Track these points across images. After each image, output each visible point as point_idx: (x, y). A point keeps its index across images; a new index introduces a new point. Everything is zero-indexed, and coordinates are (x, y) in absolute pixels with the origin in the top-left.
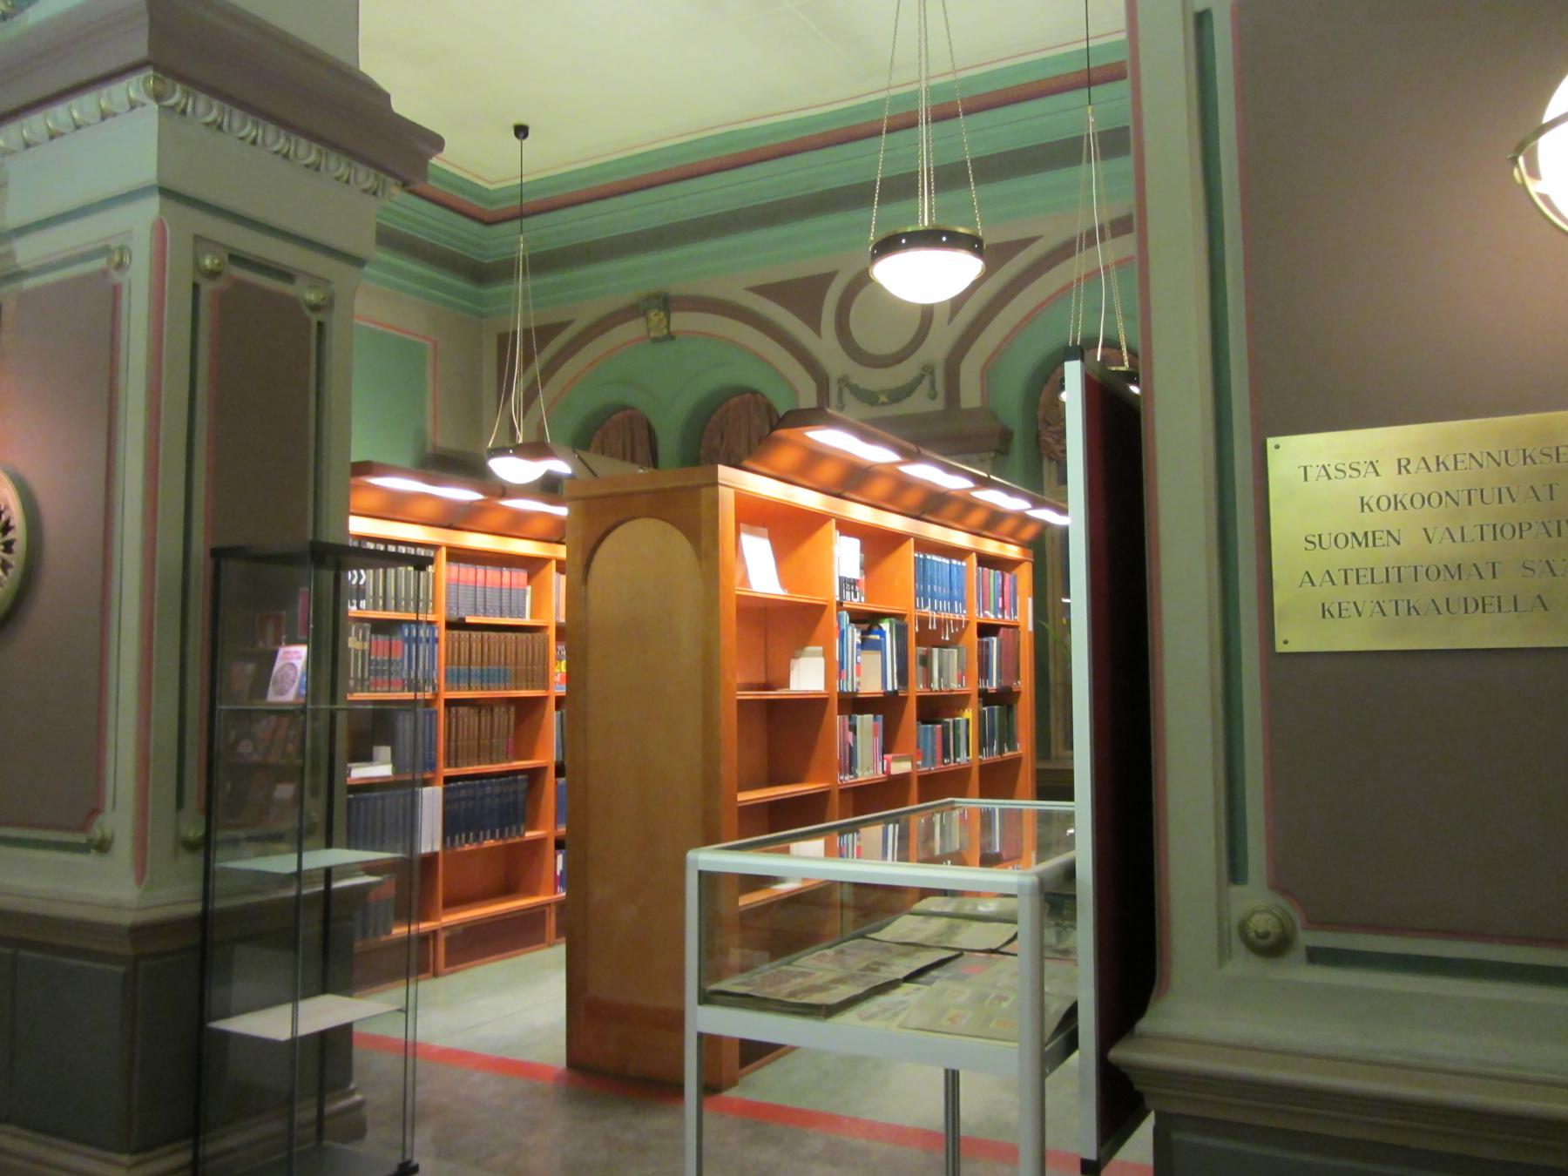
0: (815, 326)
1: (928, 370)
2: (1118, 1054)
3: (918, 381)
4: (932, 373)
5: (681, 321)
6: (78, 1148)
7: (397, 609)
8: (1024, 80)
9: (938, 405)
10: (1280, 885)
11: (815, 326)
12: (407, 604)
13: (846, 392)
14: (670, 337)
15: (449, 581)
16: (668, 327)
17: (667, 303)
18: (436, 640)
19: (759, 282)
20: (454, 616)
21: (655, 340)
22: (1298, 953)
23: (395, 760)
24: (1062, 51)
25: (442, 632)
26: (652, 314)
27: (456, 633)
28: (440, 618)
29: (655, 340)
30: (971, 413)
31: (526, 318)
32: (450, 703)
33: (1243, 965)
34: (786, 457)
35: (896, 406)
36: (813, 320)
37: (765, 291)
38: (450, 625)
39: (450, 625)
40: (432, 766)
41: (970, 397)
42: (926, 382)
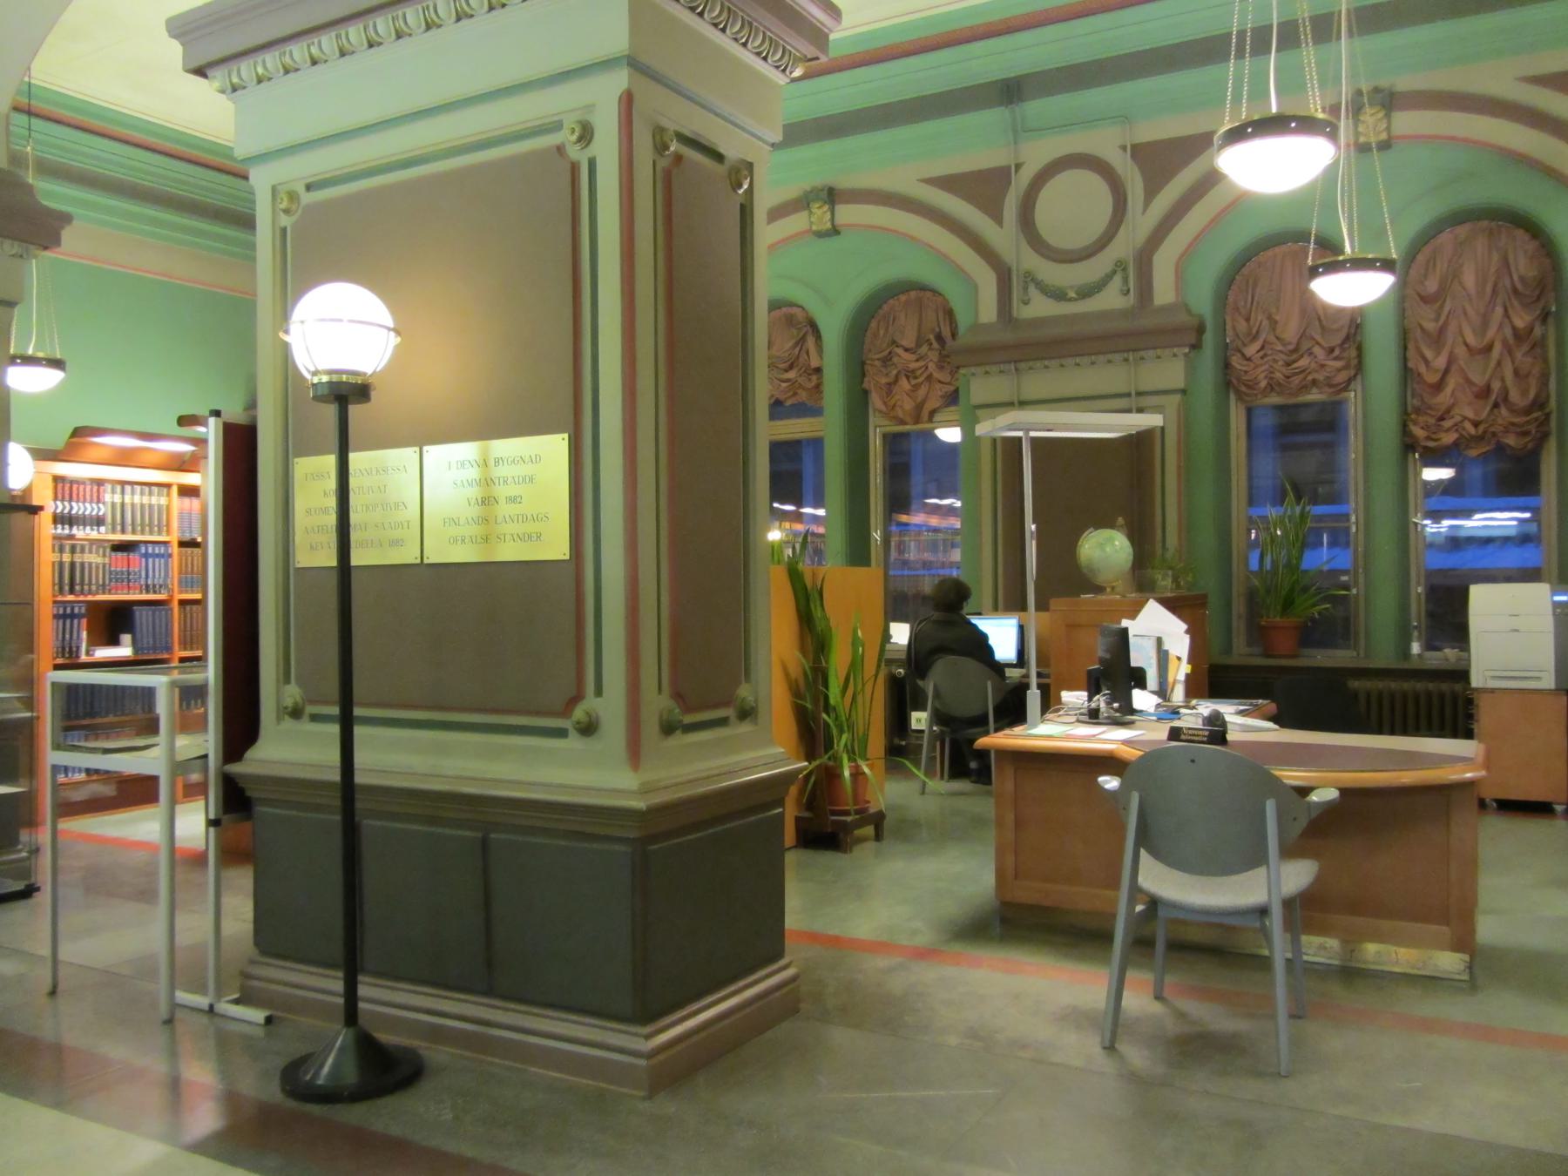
0: (998, 219)
1: (1120, 265)
2: (235, 768)
3: (1108, 278)
4: (1124, 269)
5: (847, 213)
6: (550, 1013)
7: (134, 532)
8: (923, 34)
9: (1131, 300)
10: (300, 683)
11: (998, 219)
12: (159, 526)
13: (1032, 289)
14: (835, 231)
15: (181, 514)
16: (1388, 129)
17: (832, 196)
18: (170, 556)
19: (927, 176)
20: (187, 537)
21: (820, 235)
22: (306, 717)
23: (134, 643)
24: (897, 21)
25: (175, 549)
26: (815, 206)
27: (189, 550)
28: (174, 539)
29: (820, 235)
30: (1165, 309)
31: (1353, 75)
32: (183, 603)
33: (289, 723)
34: (93, 453)
35: (1081, 303)
36: (994, 212)
37: (948, 183)
38: (182, 544)
39: (182, 544)
40: (169, 649)
41: (1164, 292)
42: (1117, 279)
